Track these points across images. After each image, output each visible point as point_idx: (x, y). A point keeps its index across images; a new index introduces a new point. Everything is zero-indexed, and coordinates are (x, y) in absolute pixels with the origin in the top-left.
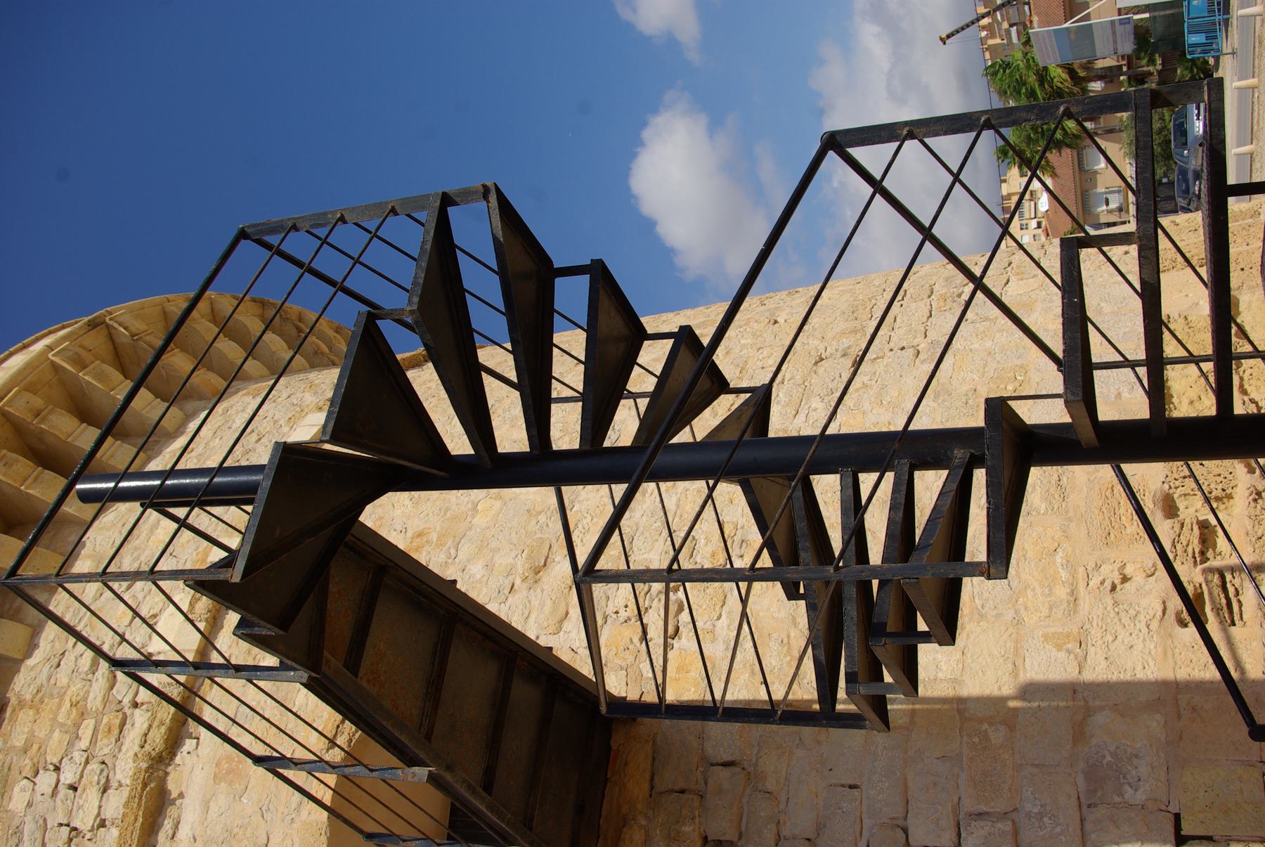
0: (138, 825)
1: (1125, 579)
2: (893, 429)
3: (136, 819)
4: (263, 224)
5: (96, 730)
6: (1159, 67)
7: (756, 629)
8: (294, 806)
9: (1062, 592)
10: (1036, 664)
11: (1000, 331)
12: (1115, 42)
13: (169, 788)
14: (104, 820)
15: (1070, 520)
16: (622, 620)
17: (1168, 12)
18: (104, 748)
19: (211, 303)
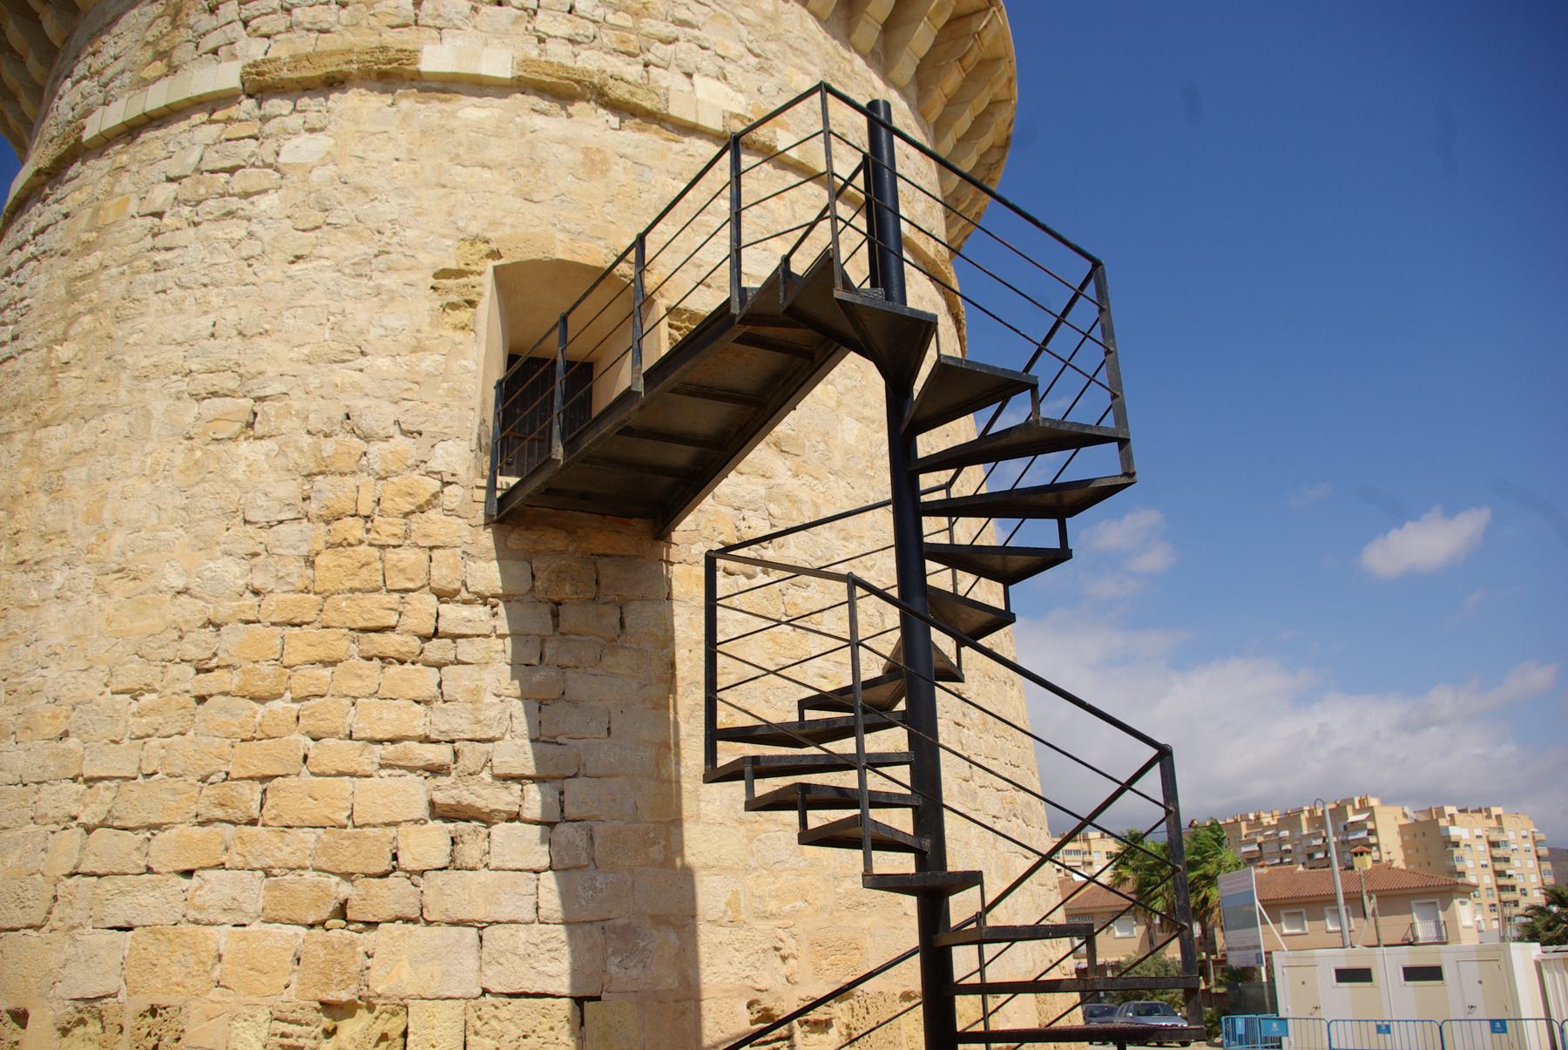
0: (544, 78)
1: (784, 958)
2: (944, 795)
3: (548, 75)
4: (1105, 283)
5: (623, 28)
6: (1214, 990)
7: (736, 645)
8: (567, 226)
9: (772, 906)
10: (714, 885)
11: (986, 852)
12: (1240, 949)
13: (576, 104)
14: (544, 41)
15: (831, 913)
16: (738, 523)
17: (1267, 1000)
18: (608, 38)
19: (1006, 101)
